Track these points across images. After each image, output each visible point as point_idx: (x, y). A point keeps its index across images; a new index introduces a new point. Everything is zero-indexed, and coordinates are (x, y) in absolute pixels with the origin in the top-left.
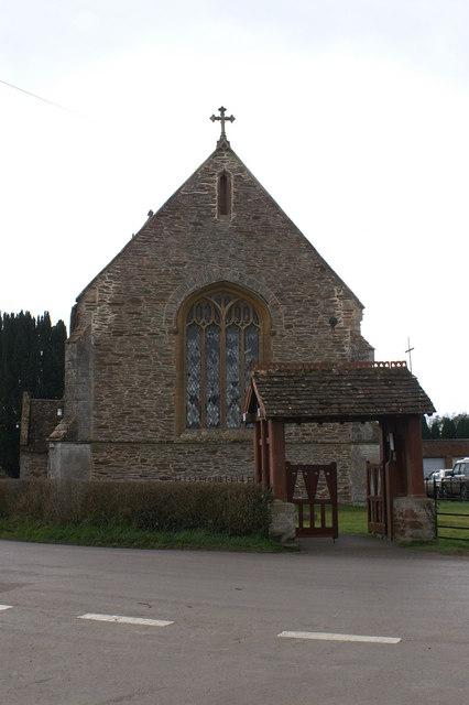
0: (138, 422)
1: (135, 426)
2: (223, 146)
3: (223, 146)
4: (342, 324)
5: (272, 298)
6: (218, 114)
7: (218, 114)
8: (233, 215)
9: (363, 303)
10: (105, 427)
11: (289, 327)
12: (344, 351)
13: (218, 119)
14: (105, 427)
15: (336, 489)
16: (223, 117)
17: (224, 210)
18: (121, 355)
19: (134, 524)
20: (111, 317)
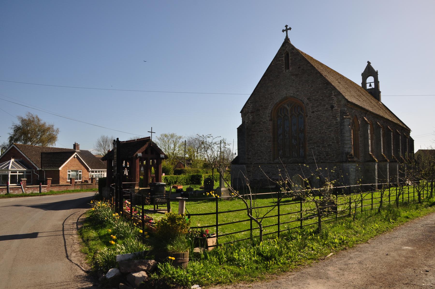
0: (260, 156)
1: (260, 158)
2: (287, 40)
3: (287, 40)
4: (336, 108)
5: (306, 101)
6: (288, 27)
7: (285, 28)
8: (290, 68)
9: (149, 136)
10: (250, 158)
11: (313, 112)
12: (337, 120)
13: (286, 28)
14: (250, 158)
15: (218, 232)
16: (287, 29)
17: (287, 67)
18: (254, 131)
19: (87, 261)
20: (251, 117)
